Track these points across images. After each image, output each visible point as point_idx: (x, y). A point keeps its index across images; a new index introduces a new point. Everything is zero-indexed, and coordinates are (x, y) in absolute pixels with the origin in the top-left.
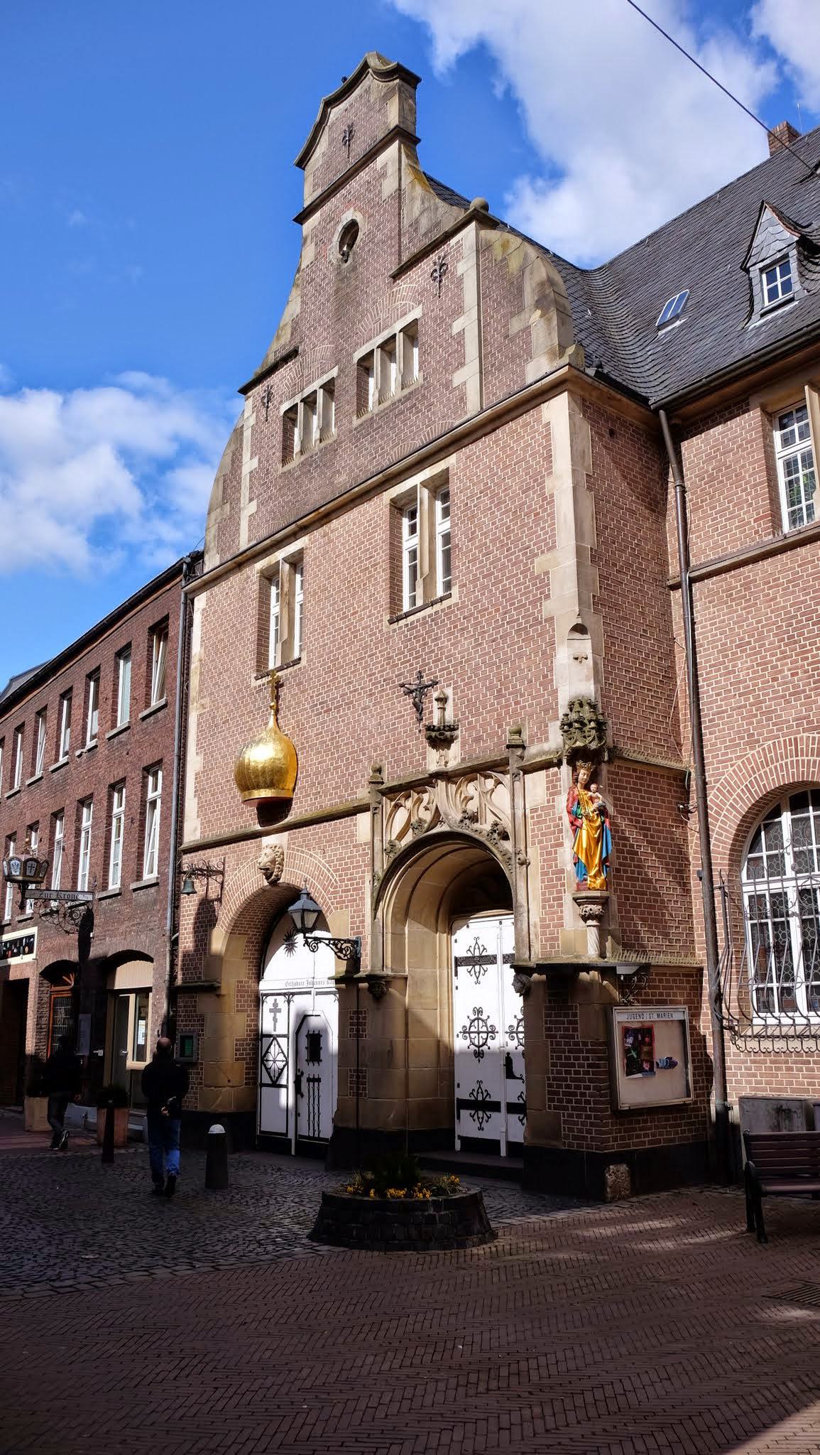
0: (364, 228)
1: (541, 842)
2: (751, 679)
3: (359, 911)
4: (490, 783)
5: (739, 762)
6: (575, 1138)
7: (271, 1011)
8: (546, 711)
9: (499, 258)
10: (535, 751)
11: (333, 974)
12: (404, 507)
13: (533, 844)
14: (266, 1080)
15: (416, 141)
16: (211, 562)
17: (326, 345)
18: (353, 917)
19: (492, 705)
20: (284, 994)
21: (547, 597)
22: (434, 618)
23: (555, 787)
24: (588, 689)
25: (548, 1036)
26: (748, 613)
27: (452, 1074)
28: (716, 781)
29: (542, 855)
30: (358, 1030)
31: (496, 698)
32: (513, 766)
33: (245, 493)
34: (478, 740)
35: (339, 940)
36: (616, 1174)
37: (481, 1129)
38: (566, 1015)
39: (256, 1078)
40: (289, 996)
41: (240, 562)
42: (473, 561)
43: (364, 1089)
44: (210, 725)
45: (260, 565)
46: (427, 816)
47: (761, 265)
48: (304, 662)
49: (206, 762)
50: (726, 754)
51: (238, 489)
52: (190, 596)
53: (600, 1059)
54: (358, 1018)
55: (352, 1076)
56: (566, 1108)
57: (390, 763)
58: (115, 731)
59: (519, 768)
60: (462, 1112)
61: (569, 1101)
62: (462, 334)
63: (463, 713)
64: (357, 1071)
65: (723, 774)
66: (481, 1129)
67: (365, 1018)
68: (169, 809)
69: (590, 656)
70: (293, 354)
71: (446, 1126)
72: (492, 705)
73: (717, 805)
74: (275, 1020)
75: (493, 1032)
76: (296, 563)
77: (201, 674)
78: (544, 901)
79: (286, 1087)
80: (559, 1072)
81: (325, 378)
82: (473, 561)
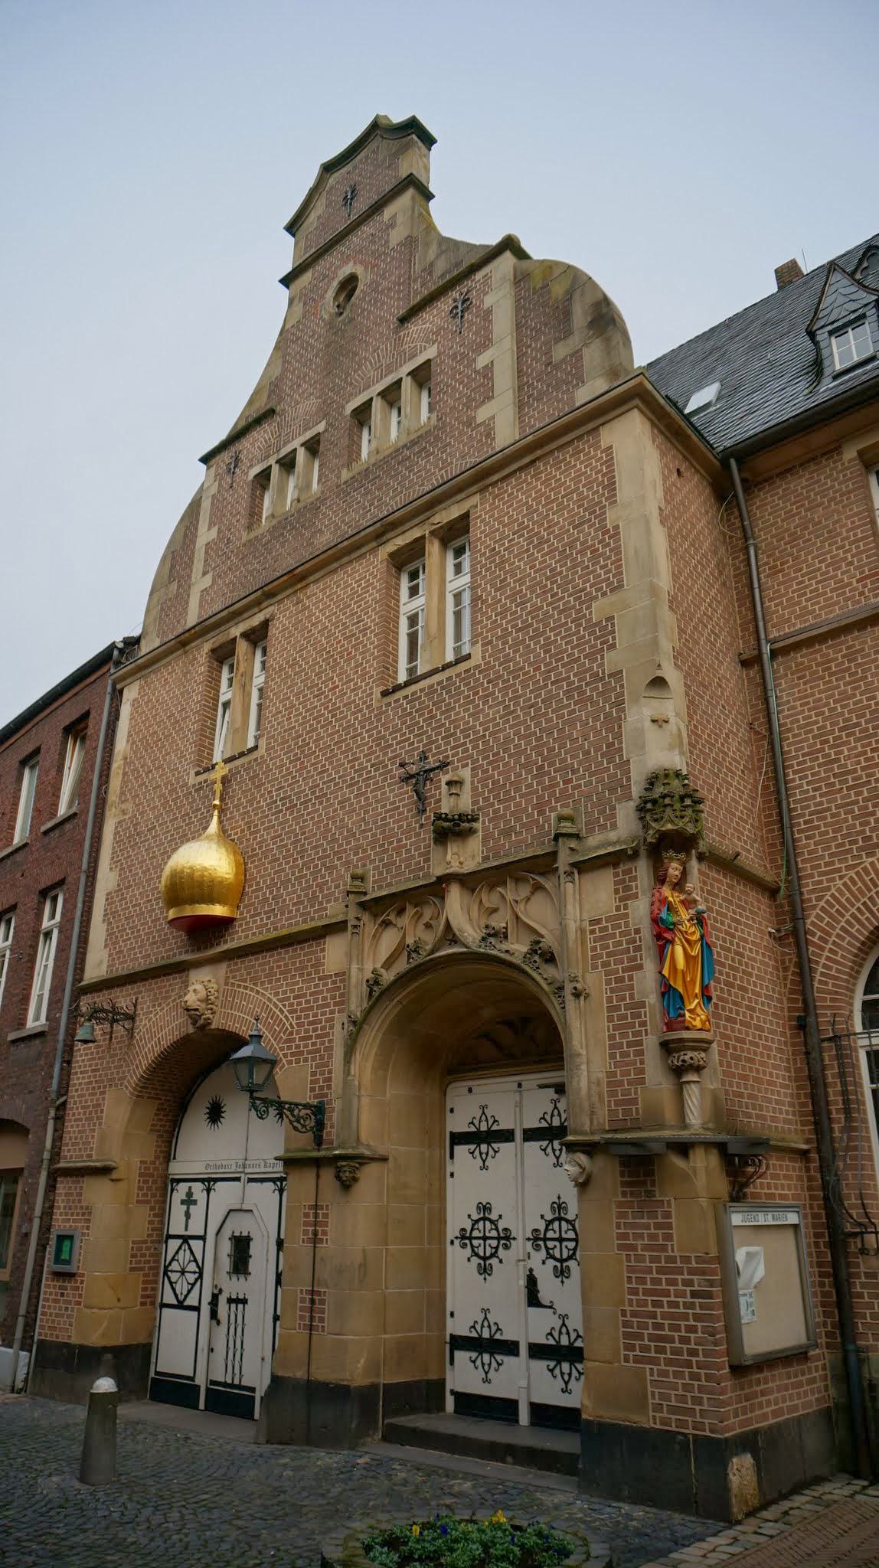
0: (365, 278)
1: (605, 964)
2: (863, 769)
3: (324, 1065)
4: (525, 891)
5: (852, 873)
6: (673, 1410)
7: (183, 1202)
8: (613, 790)
9: (539, 286)
10: (596, 843)
11: (281, 1153)
13: (595, 967)
15: (429, 196)
17: (313, 400)
18: (314, 1074)
19: (531, 786)
20: (202, 1180)
21: (613, 646)
22: (446, 686)
23: (627, 888)
25: (621, 1247)
26: (855, 689)
27: (443, 1296)
28: (819, 899)
30: (315, 1233)
31: (534, 777)
32: (564, 860)
33: (198, 566)
34: (507, 832)
35: (297, 1105)
36: (741, 1471)
37: (486, 1381)
38: (653, 1215)
39: (161, 1230)
40: (209, 1182)
42: (503, 614)
43: (322, 1320)
44: (128, 838)
46: (429, 939)
47: (830, 328)
48: (262, 751)
49: (122, 878)
50: (832, 863)
51: (189, 565)
52: (119, 687)
54: (316, 1215)
55: (303, 1300)
56: (654, 1361)
57: (376, 868)
58: (10, 850)
59: (573, 865)
61: (661, 1350)
62: (489, 368)
63: (486, 799)
64: (313, 1292)
65: (828, 889)
67: (326, 1216)
68: (69, 938)
70: (271, 413)
71: (433, 1376)
72: (531, 786)
73: (823, 930)
74: (188, 1215)
75: (507, 1238)
77: (125, 774)
78: (612, 1047)
79: (197, 1309)
80: (640, 1303)
81: (308, 435)
82: (503, 614)
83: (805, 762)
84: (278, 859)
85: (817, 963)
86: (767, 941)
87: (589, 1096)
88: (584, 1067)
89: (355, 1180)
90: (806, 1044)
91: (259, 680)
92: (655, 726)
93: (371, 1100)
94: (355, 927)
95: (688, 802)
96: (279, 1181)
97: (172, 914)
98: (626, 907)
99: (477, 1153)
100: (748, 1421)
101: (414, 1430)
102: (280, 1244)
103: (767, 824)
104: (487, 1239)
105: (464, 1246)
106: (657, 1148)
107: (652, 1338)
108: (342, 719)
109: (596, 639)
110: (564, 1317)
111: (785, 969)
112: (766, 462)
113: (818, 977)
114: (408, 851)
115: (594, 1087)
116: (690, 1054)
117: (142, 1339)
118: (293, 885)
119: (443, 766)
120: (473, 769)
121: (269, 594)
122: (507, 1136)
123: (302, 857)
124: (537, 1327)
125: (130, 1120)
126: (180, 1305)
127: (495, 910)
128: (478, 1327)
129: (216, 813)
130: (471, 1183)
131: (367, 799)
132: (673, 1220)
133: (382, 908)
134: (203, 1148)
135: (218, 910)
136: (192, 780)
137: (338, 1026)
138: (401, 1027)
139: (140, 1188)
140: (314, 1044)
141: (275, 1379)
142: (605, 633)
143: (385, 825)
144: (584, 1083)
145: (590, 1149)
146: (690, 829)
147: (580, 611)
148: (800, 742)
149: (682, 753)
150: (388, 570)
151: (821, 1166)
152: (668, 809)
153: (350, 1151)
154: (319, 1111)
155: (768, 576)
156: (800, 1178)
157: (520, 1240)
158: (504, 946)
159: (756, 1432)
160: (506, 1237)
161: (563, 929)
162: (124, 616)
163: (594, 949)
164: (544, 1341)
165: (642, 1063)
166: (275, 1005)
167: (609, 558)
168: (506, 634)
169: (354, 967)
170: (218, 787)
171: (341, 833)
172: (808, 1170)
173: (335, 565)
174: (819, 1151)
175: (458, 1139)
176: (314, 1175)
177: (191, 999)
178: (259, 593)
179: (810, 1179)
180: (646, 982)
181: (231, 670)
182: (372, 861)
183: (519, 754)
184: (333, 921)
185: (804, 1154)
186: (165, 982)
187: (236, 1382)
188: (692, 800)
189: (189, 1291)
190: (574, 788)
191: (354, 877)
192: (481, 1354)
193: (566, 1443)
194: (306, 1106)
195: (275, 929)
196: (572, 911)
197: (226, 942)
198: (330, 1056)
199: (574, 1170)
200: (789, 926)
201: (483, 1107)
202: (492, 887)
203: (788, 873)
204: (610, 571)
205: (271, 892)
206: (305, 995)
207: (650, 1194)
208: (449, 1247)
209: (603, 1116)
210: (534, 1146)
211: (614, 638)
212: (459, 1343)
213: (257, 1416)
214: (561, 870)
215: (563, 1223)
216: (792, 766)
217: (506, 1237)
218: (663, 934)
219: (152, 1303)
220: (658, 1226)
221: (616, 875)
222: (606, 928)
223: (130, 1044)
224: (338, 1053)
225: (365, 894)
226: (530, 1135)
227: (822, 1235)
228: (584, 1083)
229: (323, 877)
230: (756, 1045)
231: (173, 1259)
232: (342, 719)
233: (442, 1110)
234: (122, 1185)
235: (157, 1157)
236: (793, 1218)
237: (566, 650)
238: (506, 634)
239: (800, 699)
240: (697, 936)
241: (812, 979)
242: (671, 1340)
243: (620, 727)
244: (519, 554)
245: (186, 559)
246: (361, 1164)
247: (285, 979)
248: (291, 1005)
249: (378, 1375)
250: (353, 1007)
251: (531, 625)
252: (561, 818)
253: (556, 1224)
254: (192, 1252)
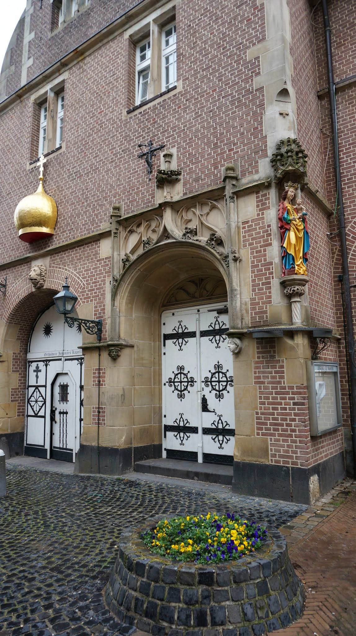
1: (250, 244)
3: (101, 302)
4: (206, 209)
7: (34, 371)
10: (246, 181)
11: (81, 345)
12: (139, 42)
13: (245, 246)
14: (31, 413)
18: (96, 307)
19: (210, 154)
20: (43, 361)
21: (259, 73)
22: (162, 105)
25: (256, 383)
27: (160, 408)
29: (252, 253)
30: (99, 381)
31: (212, 149)
32: (229, 191)
33: (25, 54)
35: (88, 321)
37: (182, 444)
38: (273, 367)
39: (25, 383)
40: (46, 362)
42: (195, 62)
43: (104, 420)
45: (34, 97)
46: (155, 237)
48: (64, 149)
51: (21, 55)
53: (304, 398)
54: (99, 373)
55: (94, 412)
56: (273, 435)
59: (233, 193)
60: (168, 433)
66: (182, 444)
67: (104, 373)
71: (156, 443)
72: (210, 154)
74: (37, 377)
75: (192, 382)
78: (253, 286)
79: (44, 417)
82: (195, 62)
83: (350, 148)
84: (74, 203)
85: (350, 249)
86: (326, 238)
87: (241, 310)
88: (238, 296)
89: (119, 356)
90: (342, 289)
91: (61, 113)
92: (281, 117)
93: (123, 319)
94: (115, 233)
95: (300, 155)
96: (80, 360)
97: (21, 232)
98: (263, 214)
99: (177, 343)
100: (317, 460)
101: (149, 467)
102: (82, 387)
103: (327, 181)
104: (182, 382)
105: (171, 386)
106: (280, 335)
107: (271, 424)
108: (106, 128)
109: (249, 70)
110: (220, 416)
111: (333, 253)
113: (350, 256)
114: (143, 193)
115: (243, 306)
116: (297, 287)
117: (19, 430)
118: (82, 216)
119: (162, 147)
120: (178, 148)
121: (64, 65)
122: (192, 335)
123: (87, 201)
124: (208, 421)
125: (7, 333)
126: (36, 416)
127: (190, 221)
128: (178, 421)
129: (41, 182)
130: (173, 357)
131: (120, 168)
132: (285, 369)
133: (128, 224)
134: (42, 346)
135: (44, 230)
136: (28, 167)
137: (108, 284)
138: (138, 284)
139: (14, 365)
140: (95, 293)
141: (82, 446)
142: (254, 67)
143: (130, 181)
144: (238, 304)
145: (240, 336)
146: (301, 169)
147: (240, 55)
148: (348, 138)
149: (295, 133)
150: (129, 45)
151: (346, 346)
152: (290, 159)
153: (116, 342)
154: (99, 324)
155: (336, 48)
156: (336, 352)
157: (199, 382)
158: (195, 238)
159: (319, 465)
160: (192, 381)
161: (229, 226)
163: (244, 237)
164: (211, 427)
165: (270, 293)
166: (75, 275)
167: (258, 23)
168: (196, 73)
169: (116, 254)
170: (42, 169)
171: (107, 187)
172: (339, 347)
173: (100, 44)
174: (345, 339)
175: (167, 337)
176: (97, 355)
177: (33, 274)
178: (59, 64)
179: (340, 352)
180: (274, 253)
181: (46, 110)
182: (124, 200)
183: (203, 137)
184: (104, 231)
185: (338, 340)
186: (20, 269)
187: (65, 447)
188: (300, 155)
189: (40, 410)
190: (234, 153)
191: (115, 208)
192: (179, 433)
193: (226, 471)
194: (93, 322)
195: (74, 238)
196: (234, 217)
197: (49, 246)
198: (104, 298)
199: (233, 346)
200: (336, 231)
201: (180, 322)
202: (188, 209)
203: (338, 205)
204: (258, 31)
205: (71, 220)
206: (90, 270)
207: (274, 357)
208: (163, 387)
209: (248, 320)
210: (206, 339)
211: (259, 69)
212: (168, 428)
213: (74, 461)
214: (227, 197)
215: (220, 374)
216: (343, 151)
217: (192, 381)
218: (284, 225)
219: (23, 415)
220: (276, 372)
221: (257, 197)
222: (251, 226)
223: (4, 299)
224: (108, 296)
225: (120, 217)
226: (204, 334)
227: (345, 377)
228: (238, 304)
229: (98, 210)
230: (322, 287)
231: (31, 396)
232: (106, 128)
233: (159, 324)
234: (5, 364)
235: (21, 351)
236: (335, 370)
237: (231, 78)
238: (196, 73)
239: (349, 115)
240: (302, 227)
241: (348, 257)
242: (282, 425)
243: (262, 118)
244: (204, 27)
245: (19, 52)
246: (121, 349)
247: (80, 262)
248: (83, 275)
249: (131, 444)
250: (115, 273)
251: (211, 66)
252: (228, 169)
253: (217, 375)
254: (40, 393)
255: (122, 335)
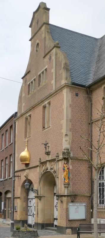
11: (34, 196)
16: (19, 115)
24: (68, 146)
32: (57, 160)
41: (22, 115)
69: (68, 140)
71: (52, 223)
76: (30, 116)
112: (94, 87)
117: (26, 219)
126: (30, 215)
129: (26, 146)
162: (14, 109)
255: (42, 194)
